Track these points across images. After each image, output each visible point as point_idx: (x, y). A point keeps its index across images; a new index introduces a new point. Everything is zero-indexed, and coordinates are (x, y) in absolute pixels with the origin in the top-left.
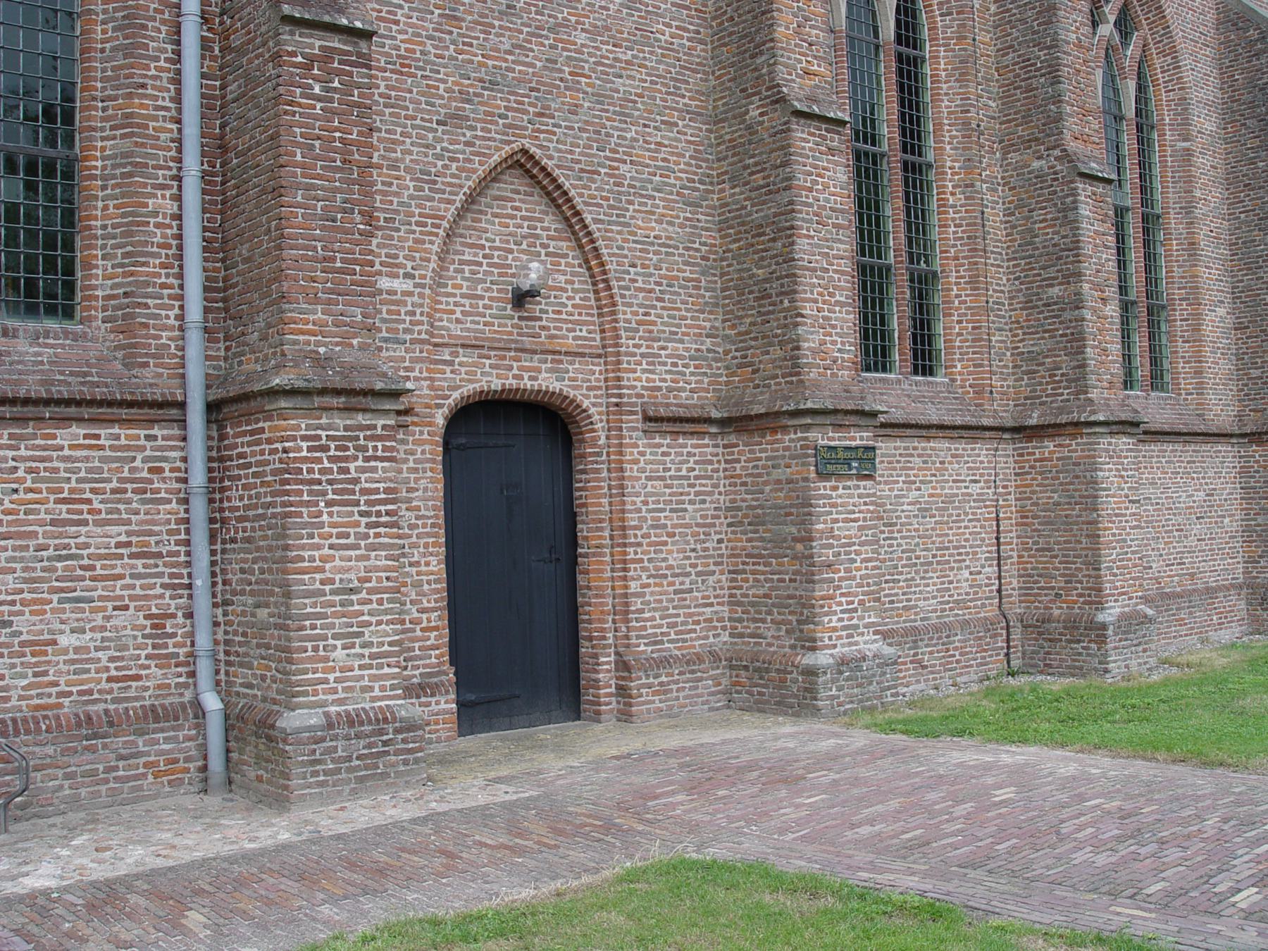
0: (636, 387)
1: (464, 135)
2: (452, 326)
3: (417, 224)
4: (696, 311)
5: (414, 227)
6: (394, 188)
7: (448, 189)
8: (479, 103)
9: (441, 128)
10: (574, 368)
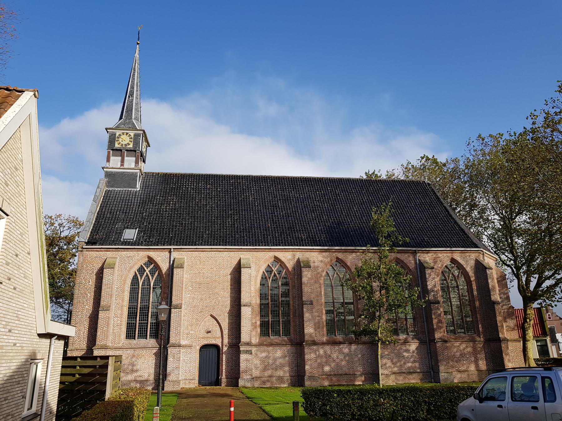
10: (218, 340)
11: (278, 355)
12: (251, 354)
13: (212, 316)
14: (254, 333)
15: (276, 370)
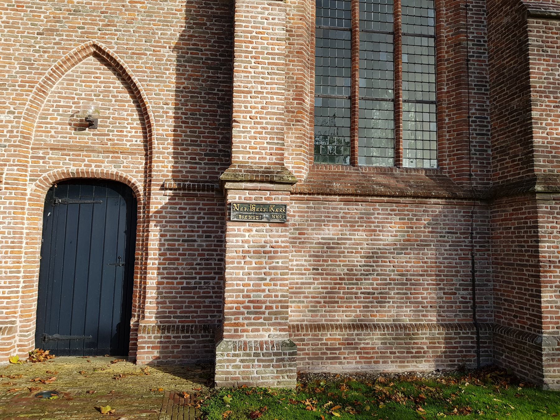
0: (163, 171)
1: (55, 39)
2: (48, 139)
3: (19, 86)
4: (212, 129)
5: (17, 88)
6: (7, 69)
7: (41, 67)
8: (67, 22)
9: (39, 37)
10: (126, 161)
11: (390, 239)
12: (283, 223)
13: (101, 55)
14: (290, 139)
15: (380, 299)
